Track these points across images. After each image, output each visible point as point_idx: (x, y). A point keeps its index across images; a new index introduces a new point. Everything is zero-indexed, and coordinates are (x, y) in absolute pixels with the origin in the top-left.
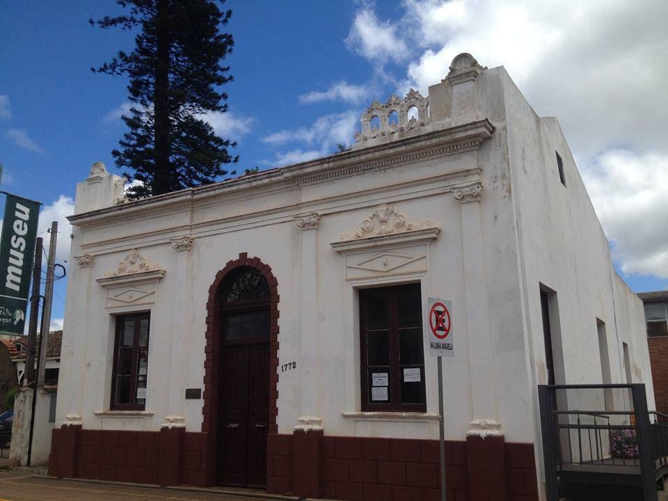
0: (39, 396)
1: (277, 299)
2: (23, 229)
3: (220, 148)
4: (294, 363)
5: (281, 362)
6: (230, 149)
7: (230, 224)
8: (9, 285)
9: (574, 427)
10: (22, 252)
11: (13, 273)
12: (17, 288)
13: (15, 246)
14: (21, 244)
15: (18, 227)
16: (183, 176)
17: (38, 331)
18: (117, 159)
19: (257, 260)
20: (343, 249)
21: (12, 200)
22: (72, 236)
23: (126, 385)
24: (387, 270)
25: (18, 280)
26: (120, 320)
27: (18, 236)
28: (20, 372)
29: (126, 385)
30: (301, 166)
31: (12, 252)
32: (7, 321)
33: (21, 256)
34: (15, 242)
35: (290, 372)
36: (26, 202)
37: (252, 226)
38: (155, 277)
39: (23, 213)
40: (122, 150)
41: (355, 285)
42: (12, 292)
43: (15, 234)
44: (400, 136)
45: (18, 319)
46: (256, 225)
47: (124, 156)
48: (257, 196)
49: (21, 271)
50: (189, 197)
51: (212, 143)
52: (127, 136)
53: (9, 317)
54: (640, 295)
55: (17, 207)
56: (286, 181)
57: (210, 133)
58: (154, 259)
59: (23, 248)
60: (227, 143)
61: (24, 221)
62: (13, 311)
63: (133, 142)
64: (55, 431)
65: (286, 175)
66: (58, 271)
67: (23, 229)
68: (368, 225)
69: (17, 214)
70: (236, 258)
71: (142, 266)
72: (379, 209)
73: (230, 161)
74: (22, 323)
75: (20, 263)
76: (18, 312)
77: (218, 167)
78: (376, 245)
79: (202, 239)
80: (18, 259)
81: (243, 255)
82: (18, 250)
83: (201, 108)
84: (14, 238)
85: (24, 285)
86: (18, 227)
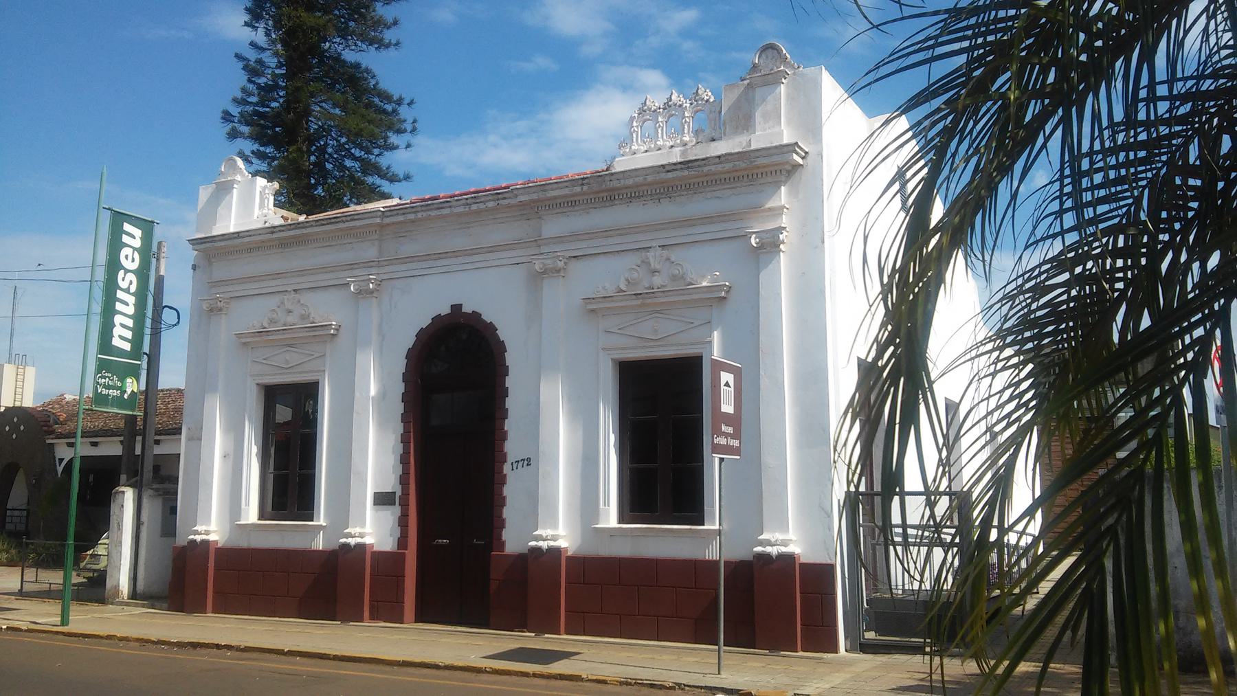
0: (145, 501)
1: (505, 371)
3: (389, 108)
4: (529, 459)
5: (511, 458)
6: (404, 111)
7: (438, 263)
8: (116, 342)
11: (122, 325)
13: (123, 285)
14: (131, 283)
15: (127, 257)
16: (330, 155)
18: (229, 127)
19: (476, 315)
20: (594, 308)
21: (119, 218)
22: (194, 267)
23: (290, 485)
24: (660, 340)
25: (129, 334)
26: (272, 395)
27: (127, 271)
28: (61, 460)
29: (290, 485)
30: (555, 198)
31: (120, 294)
32: (116, 393)
33: (131, 300)
34: (131, 283)
35: (523, 471)
36: (136, 221)
37: (470, 266)
38: (321, 335)
39: (133, 237)
40: (235, 111)
41: (616, 356)
42: (120, 352)
44: (683, 153)
45: (129, 391)
46: (477, 265)
47: (239, 122)
50: (378, 220)
51: (376, 100)
52: (244, 90)
53: (117, 388)
56: (523, 205)
57: (373, 82)
58: (327, 309)
59: (133, 289)
60: (399, 102)
61: (134, 249)
62: (122, 380)
63: (254, 99)
64: (175, 548)
65: (522, 198)
66: (168, 316)
68: (635, 275)
69: (125, 239)
70: (445, 310)
71: (304, 317)
72: (651, 254)
73: (405, 131)
75: (130, 310)
76: (129, 380)
77: (386, 138)
78: (645, 301)
79: (396, 282)
80: (121, 337)
81: (456, 308)
82: (127, 291)
83: (359, 43)
84: (121, 273)
85: (137, 341)
86: (127, 257)
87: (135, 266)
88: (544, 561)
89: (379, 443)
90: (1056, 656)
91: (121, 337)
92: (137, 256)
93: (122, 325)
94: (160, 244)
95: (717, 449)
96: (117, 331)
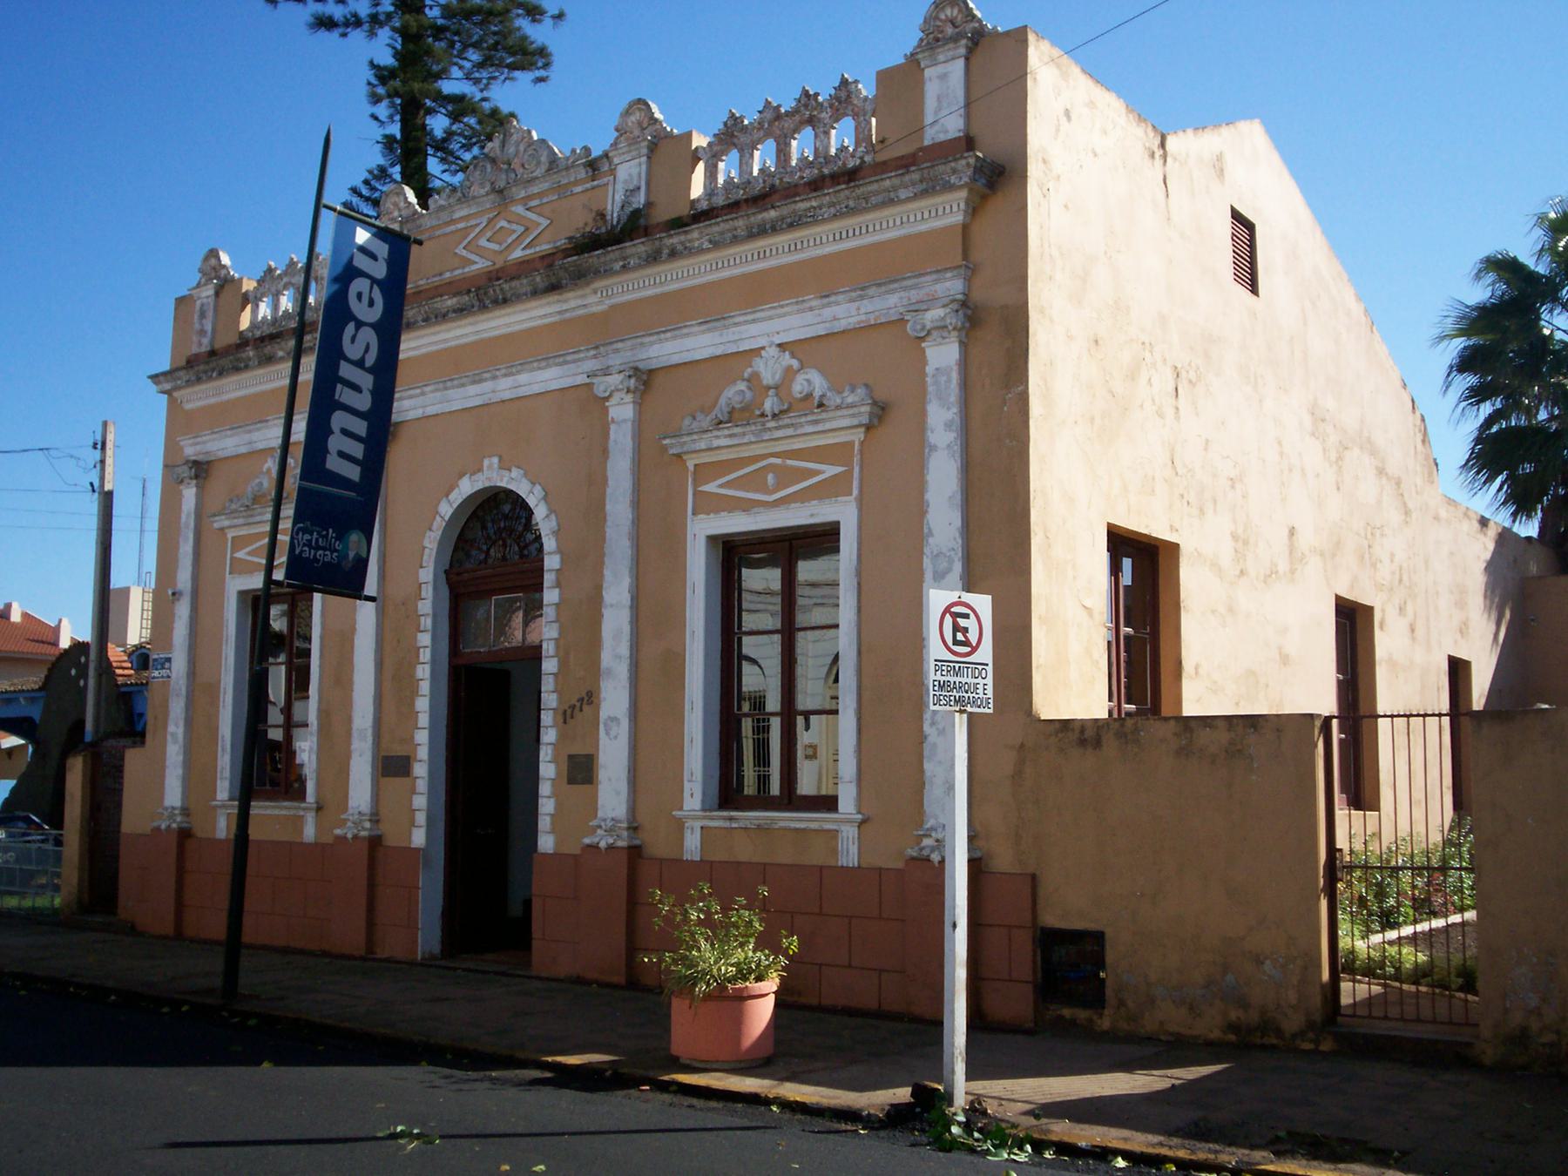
2: (371, 303)
9: (1434, 869)
10: (369, 370)
11: (345, 432)
12: (353, 473)
14: (353, 339)
15: (359, 296)
17: (548, 1075)
25: (357, 450)
27: (360, 324)
31: (346, 370)
33: (366, 381)
34: (353, 339)
42: (344, 482)
43: (353, 318)
45: (351, 554)
48: (669, 335)
49: (358, 469)
54: (1338, 598)
55: (358, 469)
61: (374, 281)
67: (371, 303)
69: (360, 427)
74: (362, 564)
80: (342, 454)
82: (360, 364)
86: (359, 296)
87: (374, 314)
88: (805, 797)
89: (948, 827)
90: (286, 392)
91: (342, 454)
92: (377, 295)
93: (345, 432)
94: (1143, 572)
95: (771, 593)
96: (336, 442)
